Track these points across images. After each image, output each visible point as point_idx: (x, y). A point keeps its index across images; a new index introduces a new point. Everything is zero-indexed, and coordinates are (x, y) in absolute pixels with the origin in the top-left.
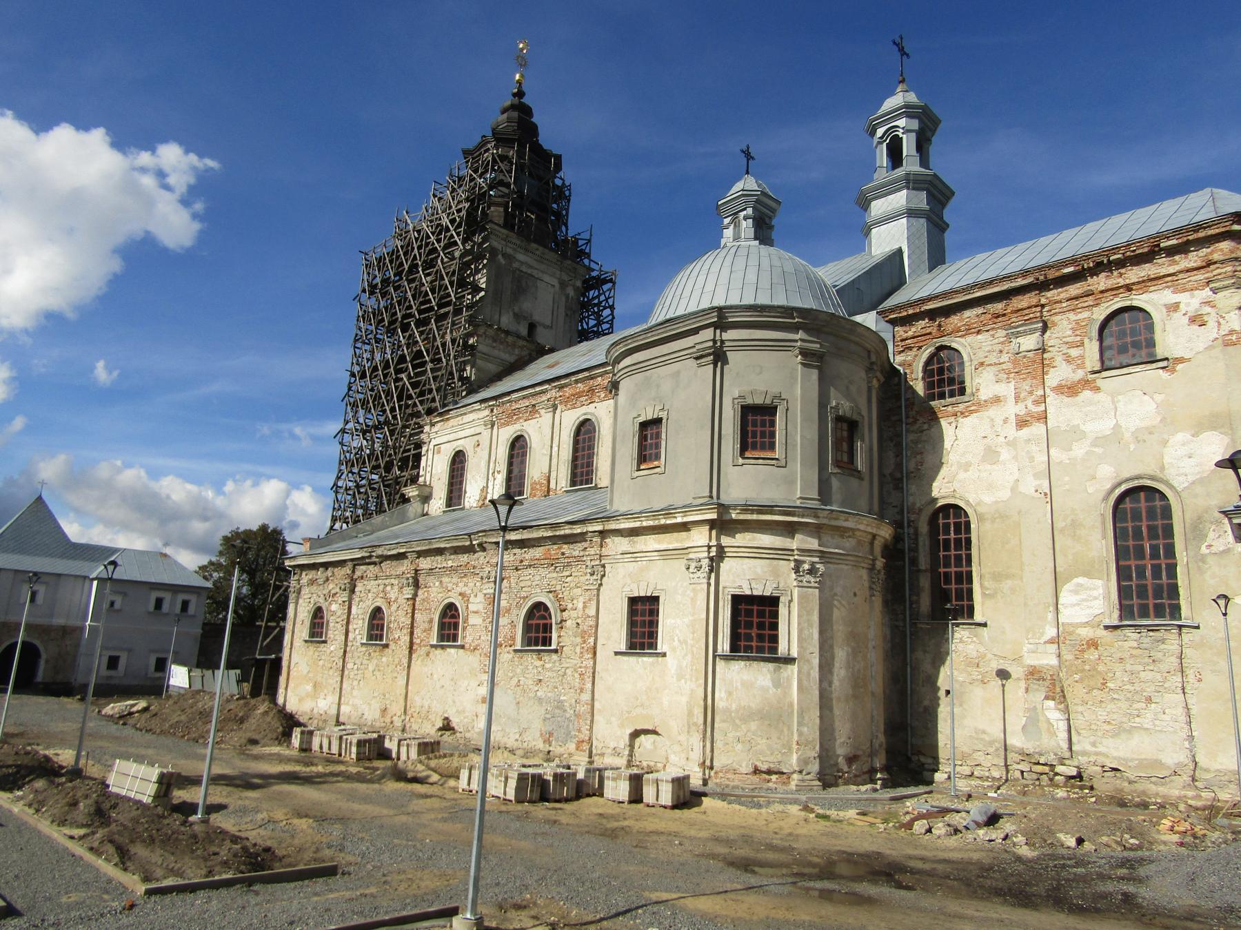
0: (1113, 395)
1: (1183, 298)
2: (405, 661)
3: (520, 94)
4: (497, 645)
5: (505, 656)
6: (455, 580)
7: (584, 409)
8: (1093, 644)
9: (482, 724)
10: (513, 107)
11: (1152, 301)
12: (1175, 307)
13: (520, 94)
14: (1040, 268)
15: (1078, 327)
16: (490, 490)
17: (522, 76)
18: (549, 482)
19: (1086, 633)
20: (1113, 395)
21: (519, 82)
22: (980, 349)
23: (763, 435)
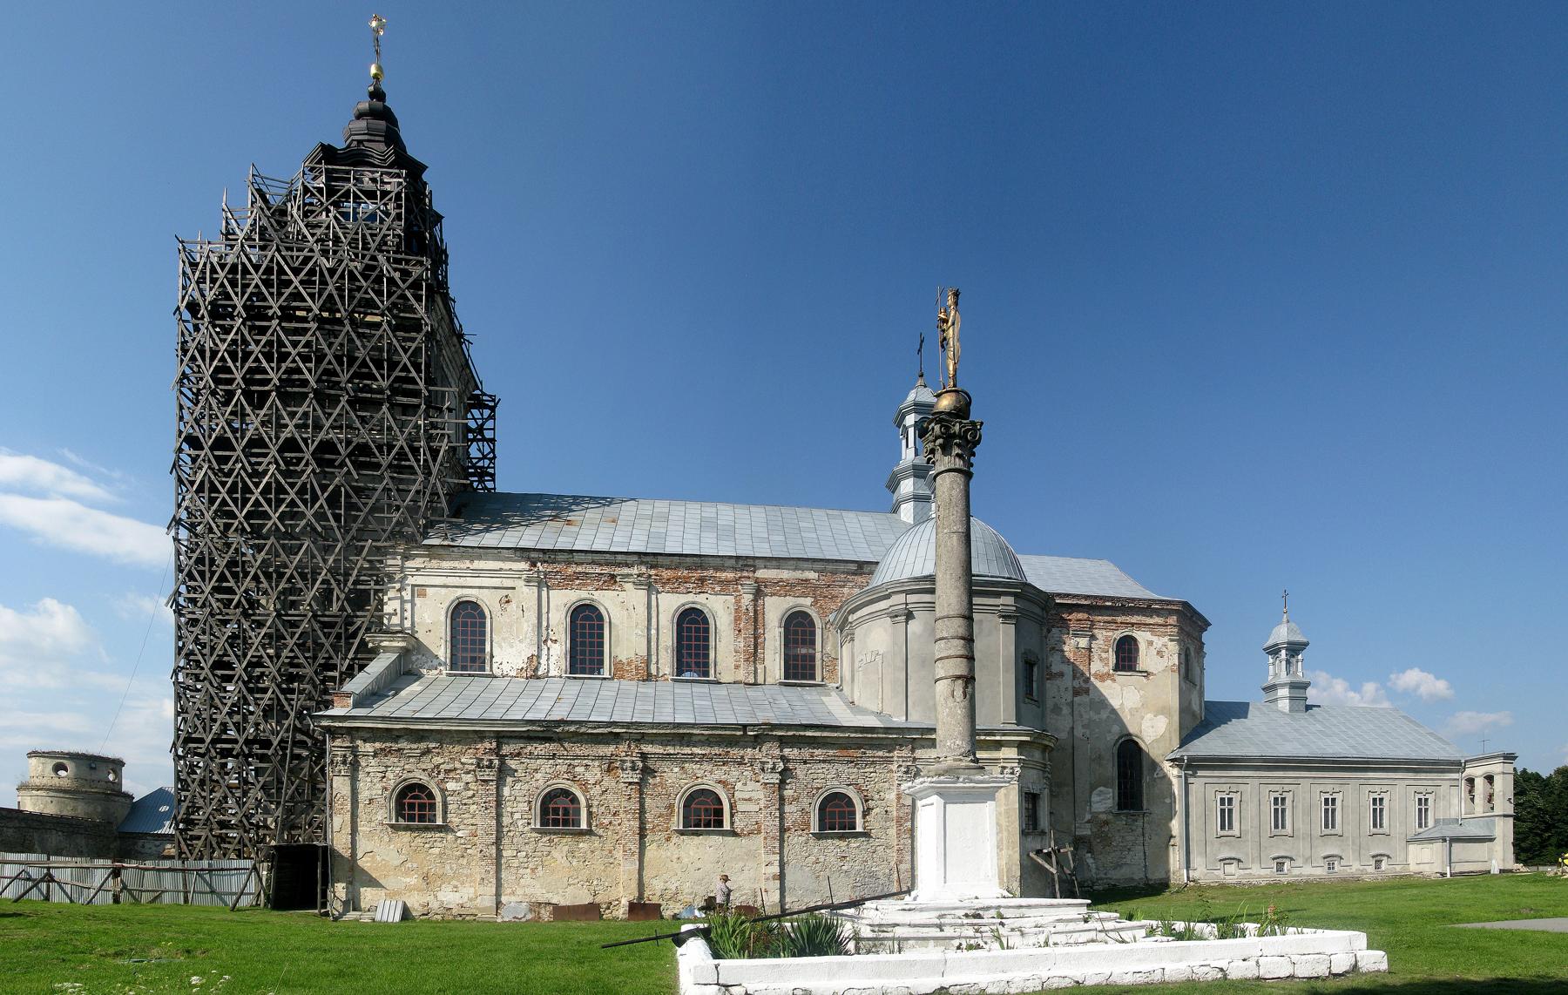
0: (1123, 686)
1: (1155, 639)
2: (635, 848)
3: (378, 95)
4: (783, 830)
5: (795, 840)
6: (709, 768)
7: (690, 597)
8: (1106, 823)
9: (776, 897)
10: (372, 113)
11: (1142, 636)
12: (1151, 643)
13: (378, 95)
14: (1096, 597)
15: (1107, 639)
16: (543, 661)
17: (379, 68)
18: (648, 666)
19: (1103, 817)
20: (1123, 686)
21: (376, 77)
22: (731, 599)
23: (591, 635)
